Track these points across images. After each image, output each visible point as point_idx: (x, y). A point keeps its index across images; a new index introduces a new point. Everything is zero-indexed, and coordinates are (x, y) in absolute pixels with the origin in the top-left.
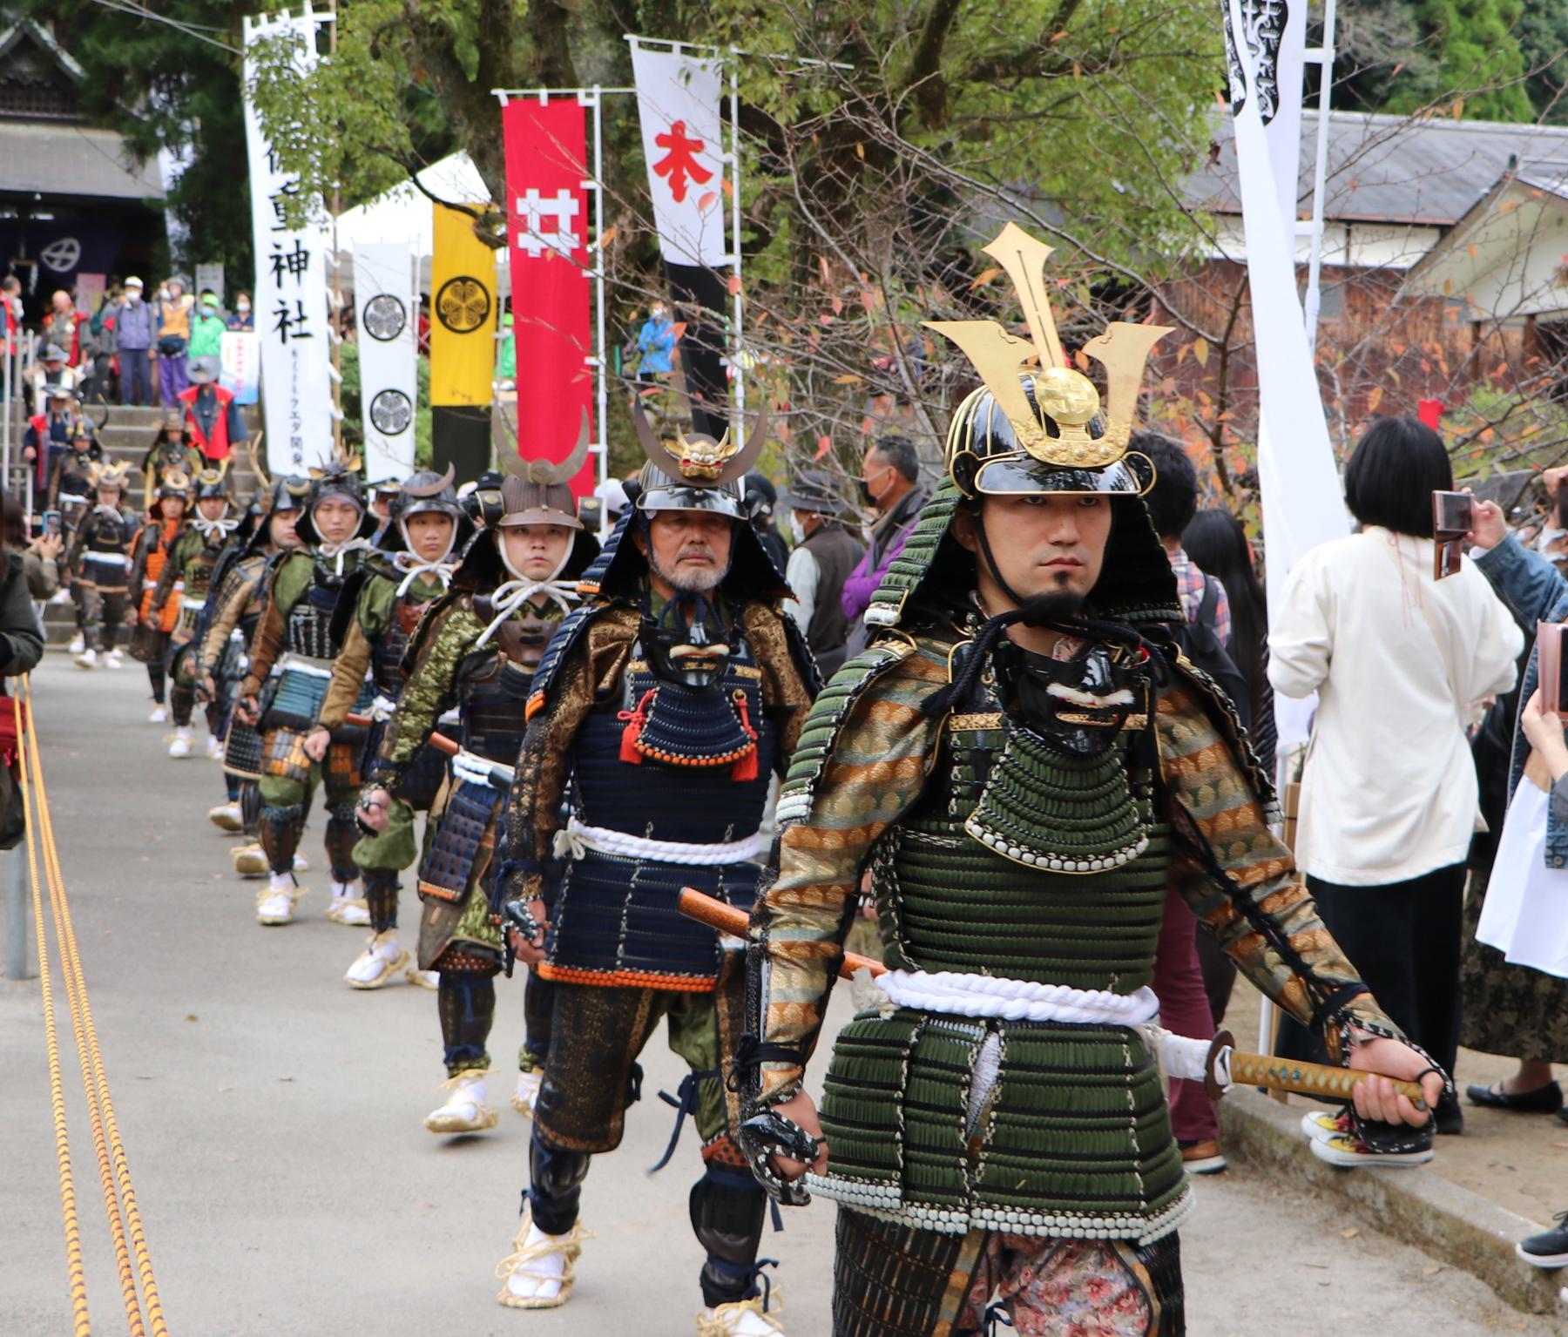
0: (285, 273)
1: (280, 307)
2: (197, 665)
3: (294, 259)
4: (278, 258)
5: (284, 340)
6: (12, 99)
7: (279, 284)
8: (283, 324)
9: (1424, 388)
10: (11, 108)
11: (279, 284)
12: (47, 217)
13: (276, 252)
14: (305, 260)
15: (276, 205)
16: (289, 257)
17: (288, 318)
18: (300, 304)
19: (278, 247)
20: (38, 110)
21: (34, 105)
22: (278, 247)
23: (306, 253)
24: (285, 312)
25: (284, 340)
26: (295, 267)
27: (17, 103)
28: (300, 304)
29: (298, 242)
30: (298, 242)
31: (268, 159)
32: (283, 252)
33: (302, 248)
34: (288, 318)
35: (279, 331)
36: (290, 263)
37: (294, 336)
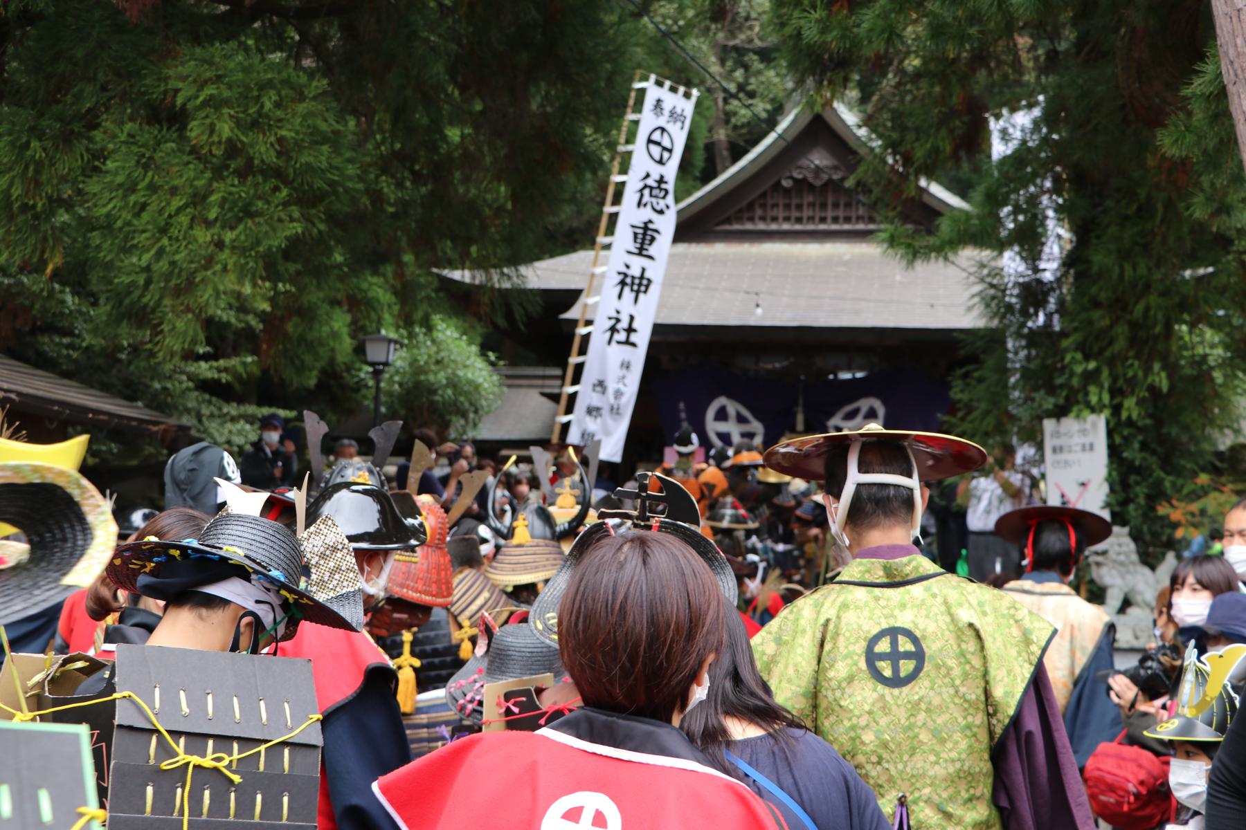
0: (627, 289)
1: (614, 314)
2: (392, 144)
3: (643, 288)
4: (626, 275)
5: (609, 342)
6: (799, 207)
7: (620, 296)
8: (613, 330)
9: (302, 339)
10: (799, 220)
11: (620, 296)
12: (845, 376)
13: (624, 270)
14: (647, 286)
15: (636, 234)
16: (633, 278)
17: (619, 326)
18: (632, 318)
19: (628, 267)
20: (835, 220)
21: (830, 214)
22: (628, 267)
23: (649, 281)
24: (618, 320)
25: (609, 342)
26: (635, 288)
27: (806, 213)
28: (632, 318)
29: (644, 270)
30: (644, 270)
31: (638, 195)
32: (630, 272)
33: (647, 275)
34: (619, 326)
35: (608, 334)
36: (633, 283)
37: (619, 343)
